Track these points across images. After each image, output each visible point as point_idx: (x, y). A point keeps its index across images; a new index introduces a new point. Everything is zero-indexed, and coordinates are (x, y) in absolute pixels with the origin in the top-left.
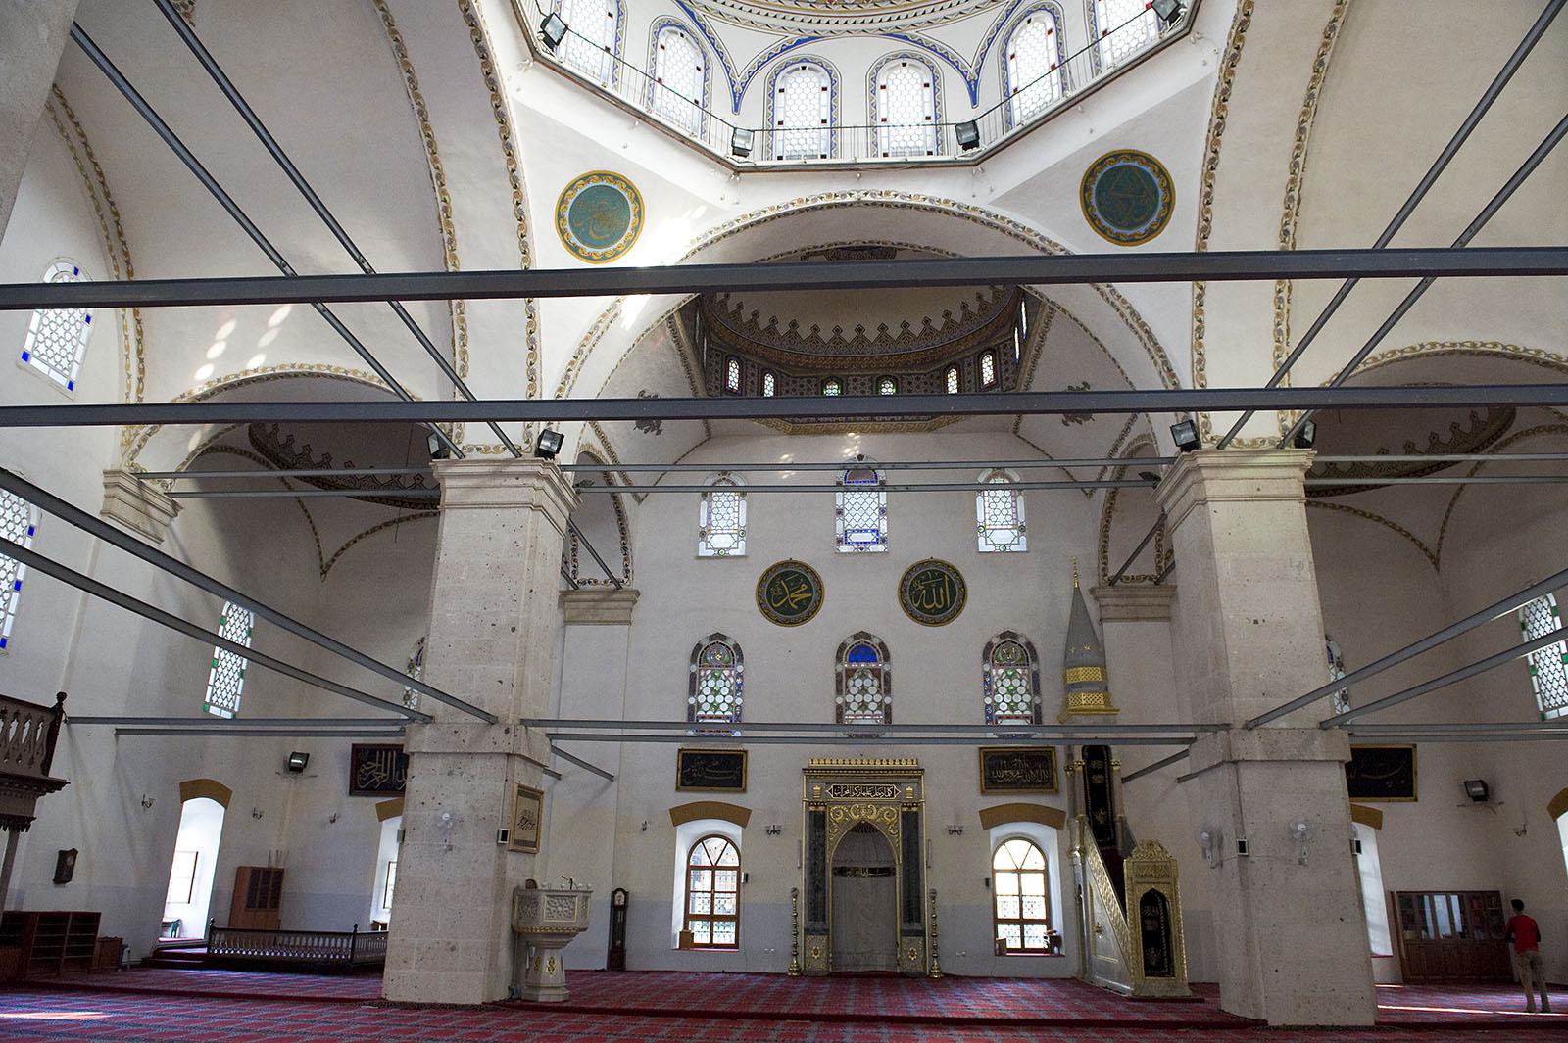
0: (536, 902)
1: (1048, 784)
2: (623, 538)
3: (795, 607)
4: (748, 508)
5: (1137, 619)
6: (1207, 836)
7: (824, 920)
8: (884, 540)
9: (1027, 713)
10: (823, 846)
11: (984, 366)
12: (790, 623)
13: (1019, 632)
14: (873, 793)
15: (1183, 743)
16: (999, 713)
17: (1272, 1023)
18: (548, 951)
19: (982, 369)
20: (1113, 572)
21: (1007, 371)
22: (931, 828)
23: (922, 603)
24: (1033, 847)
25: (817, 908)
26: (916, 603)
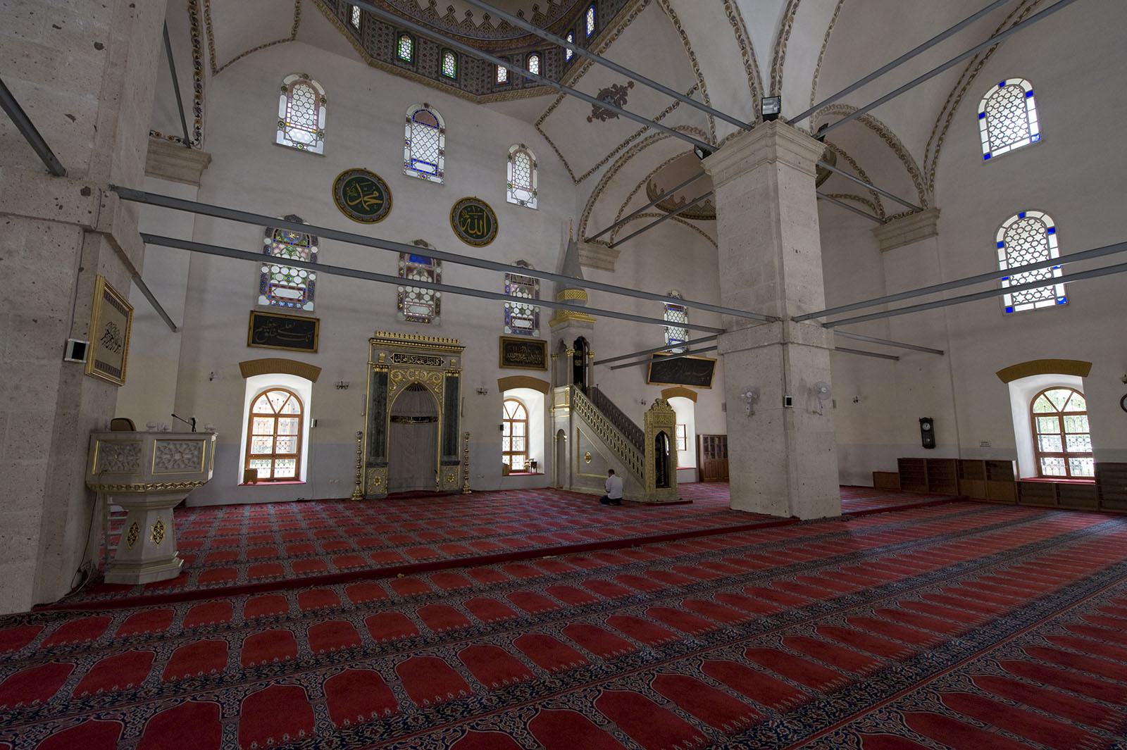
0: (135, 449)
1: (541, 365)
2: (197, 97)
3: (368, 208)
4: (328, 114)
5: (597, 267)
6: (751, 394)
7: (383, 456)
8: (441, 175)
9: (531, 317)
10: (385, 399)
11: (531, 64)
12: (362, 220)
13: (529, 262)
14: (425, 362)
15: (709, 331)
16: (513, 314)
17: (803, 518)
18: (154, 513)
19: (529, 65)
20: (589, 234)
21: (550, 71)
22: (466, 390)
23: (467, 228)
24: (520, 406)
25: (378, 447)
26: (463, 227)
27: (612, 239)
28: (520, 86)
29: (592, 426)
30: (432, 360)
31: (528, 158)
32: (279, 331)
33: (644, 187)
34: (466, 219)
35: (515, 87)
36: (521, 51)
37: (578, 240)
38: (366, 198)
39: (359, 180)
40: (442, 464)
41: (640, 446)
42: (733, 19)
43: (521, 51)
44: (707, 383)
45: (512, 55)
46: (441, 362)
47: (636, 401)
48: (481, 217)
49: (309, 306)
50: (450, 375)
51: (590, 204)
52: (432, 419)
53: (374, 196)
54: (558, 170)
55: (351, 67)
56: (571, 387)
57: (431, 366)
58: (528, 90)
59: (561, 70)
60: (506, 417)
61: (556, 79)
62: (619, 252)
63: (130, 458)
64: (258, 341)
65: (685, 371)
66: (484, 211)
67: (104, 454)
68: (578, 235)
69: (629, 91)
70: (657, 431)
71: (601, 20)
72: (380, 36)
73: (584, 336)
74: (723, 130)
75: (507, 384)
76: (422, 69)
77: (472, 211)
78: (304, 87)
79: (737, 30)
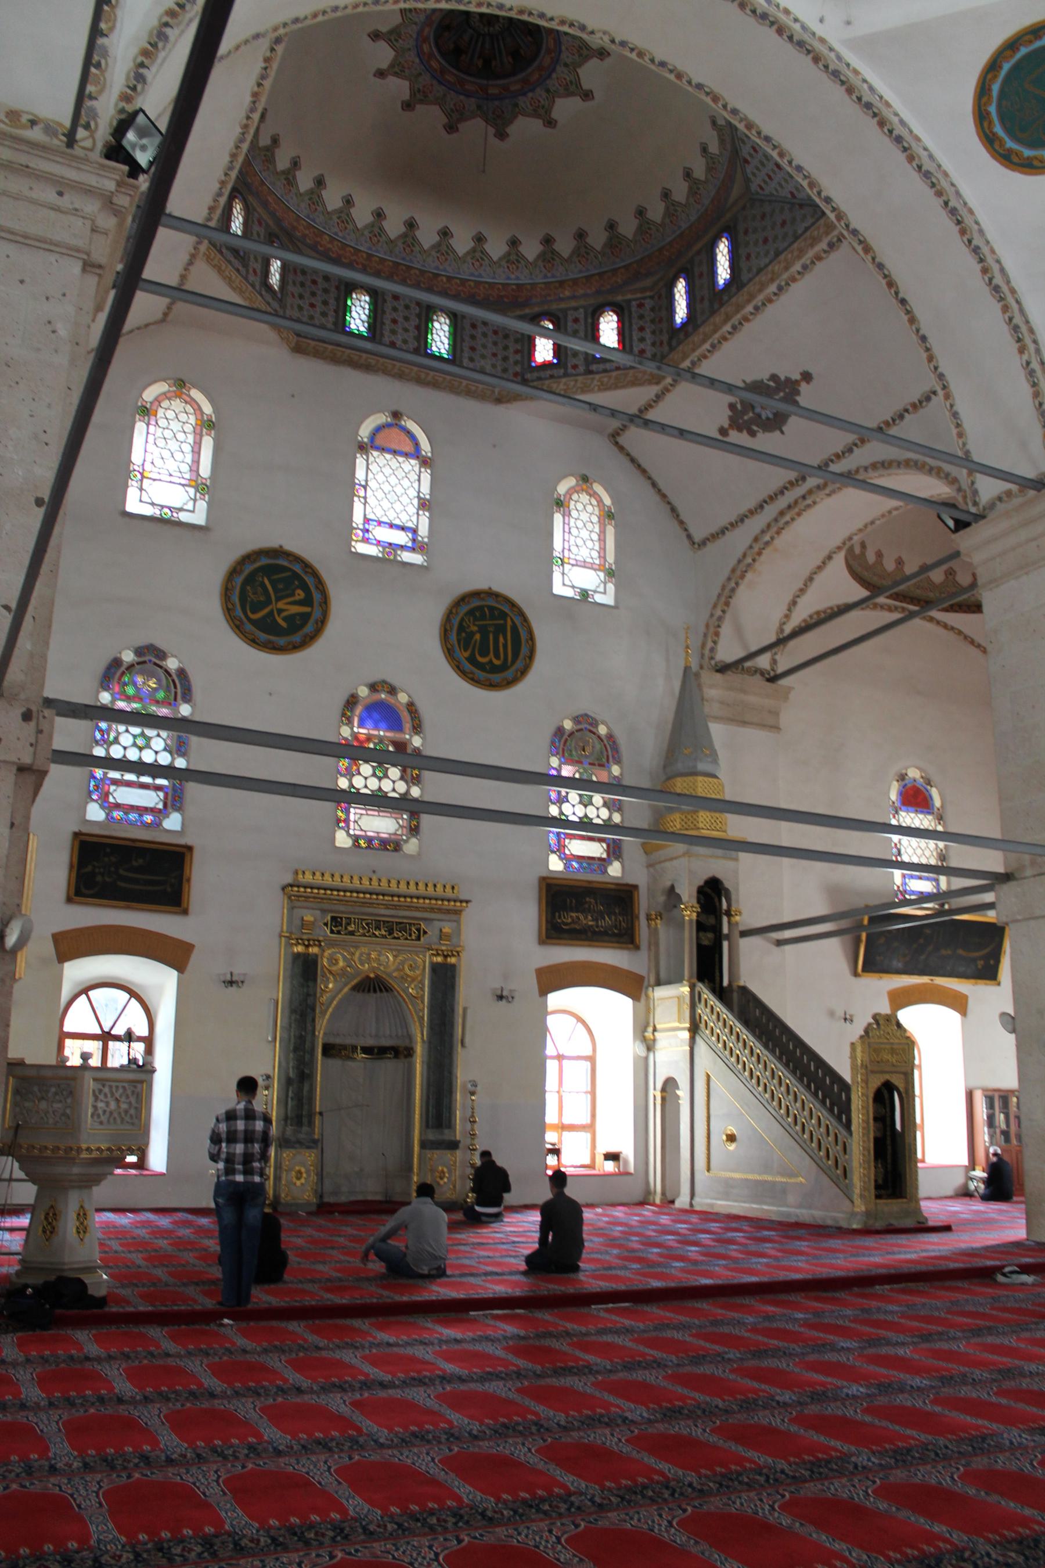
3: (284, 624)
5: (744, 723)
10: (314, 1010)
14: (391, 932)
20: (728, 651)
22: (470, 994)
27: (774, 662)
28: (582, 369)
29: (737, 1067)
30: (403, 927)
31: (594, 502)
32: (121, 872)
33: (840, 559)
34: (473, 634)
35: (570, 370)
36: (582, 302)
37: (701, 667)
38: (281, 605)
39: (269, 570)
40: (423, 1145)
41: (840, 1113)
42: (996, 289)
43: (582, 302)
44: (989, 973)
45: (565, 311)
46: (420, 933)
47: (832, 1014)
48: (501, 629)
49: (173, 822)
50: (439, 959)
51: (727, 592)
52: (402, 1052)
53: (297, 598)
54: (657, 521)
55: (258, 350)
56: (692, 987)
57: (402, 941)
58: (597, 377)
59: (659, 345)
60: (550, 1050)
61: (654, 356)
62: (790, 689)
63: (56, 1105)
64: (84, 890)
65: (947, 946)
66: (507, 615)
67: (18, 1098)
68: (703, 656)
69: (804, 387)
70: (876, 1082)
71: (743, 252)
72: (313, 294)
73: (719, 876)
74: (988, 488)
75: (554, 979)
76: (394, 346)
77: (483, 617)
78: (177, 404)
79: (1006, 308)
